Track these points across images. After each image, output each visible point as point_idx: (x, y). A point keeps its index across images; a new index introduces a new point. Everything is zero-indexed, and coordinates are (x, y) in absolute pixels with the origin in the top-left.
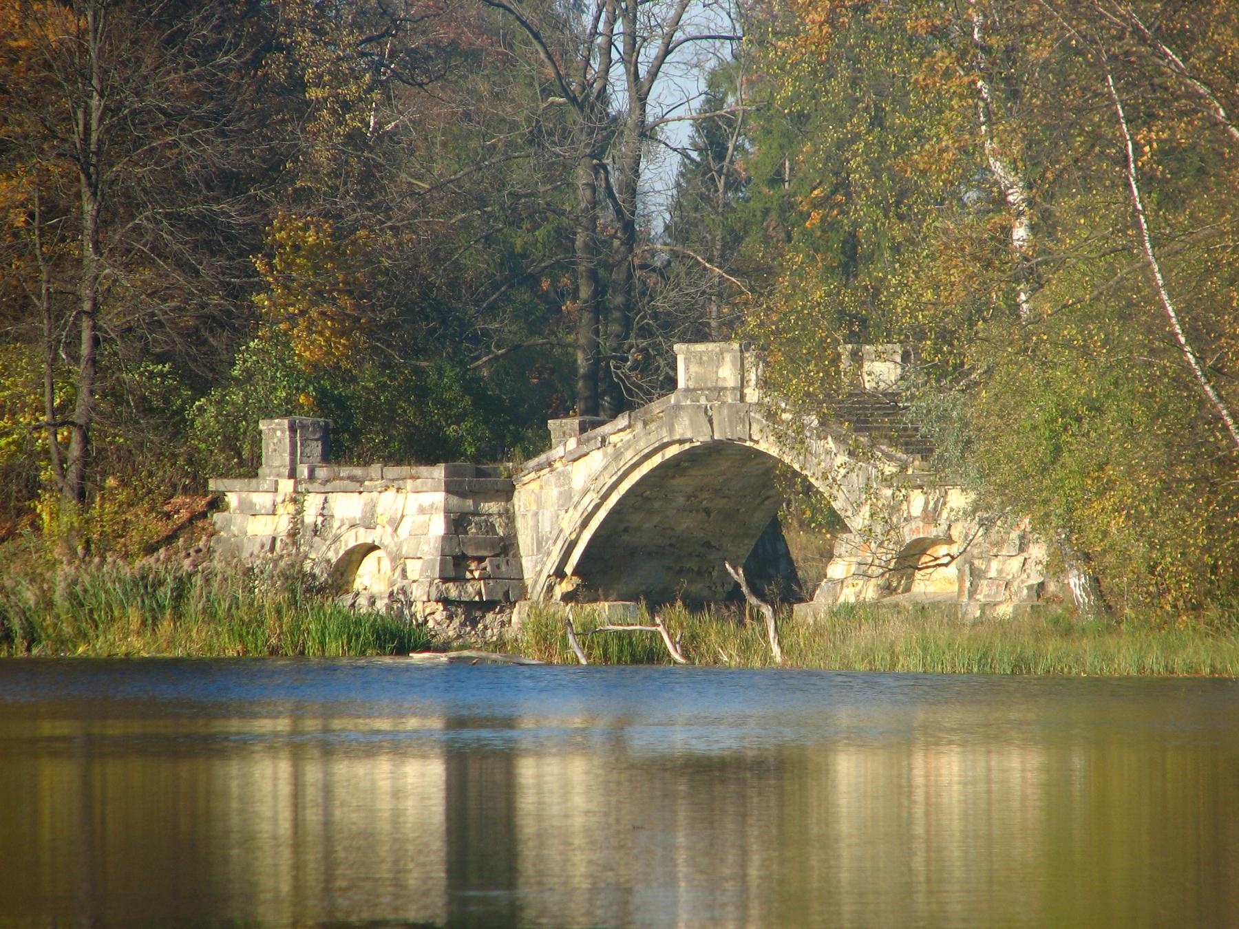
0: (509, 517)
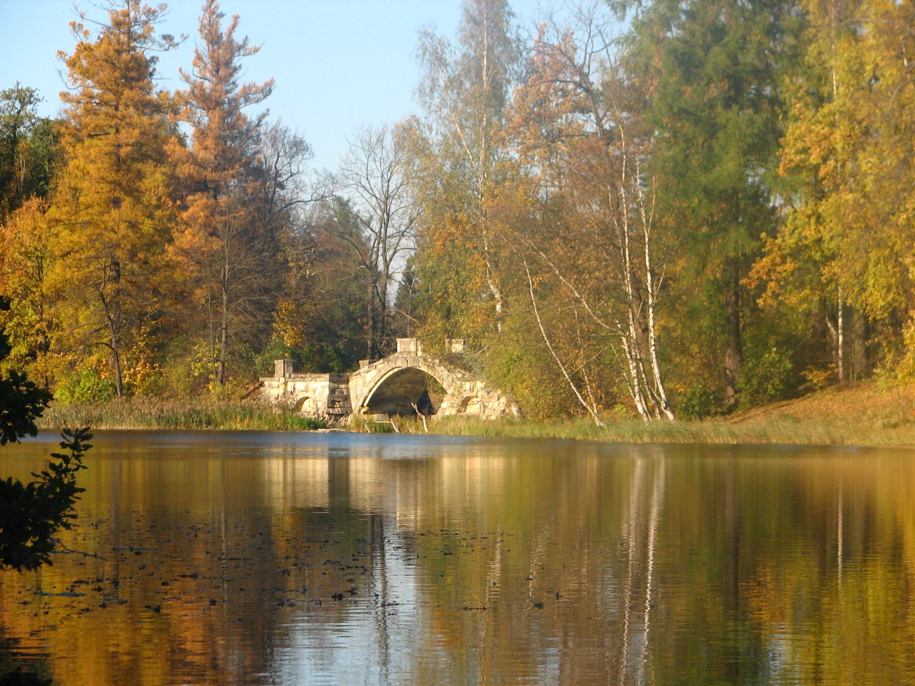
0: (348, 389)
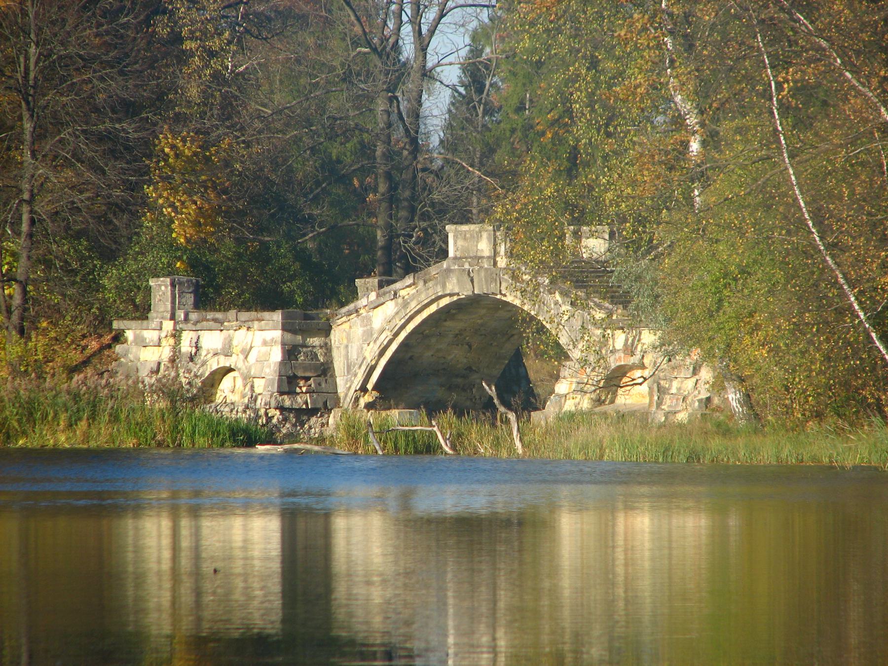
0: (327, 348)
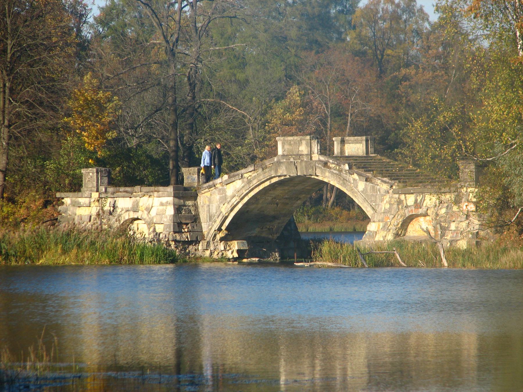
0: (196, 207)
